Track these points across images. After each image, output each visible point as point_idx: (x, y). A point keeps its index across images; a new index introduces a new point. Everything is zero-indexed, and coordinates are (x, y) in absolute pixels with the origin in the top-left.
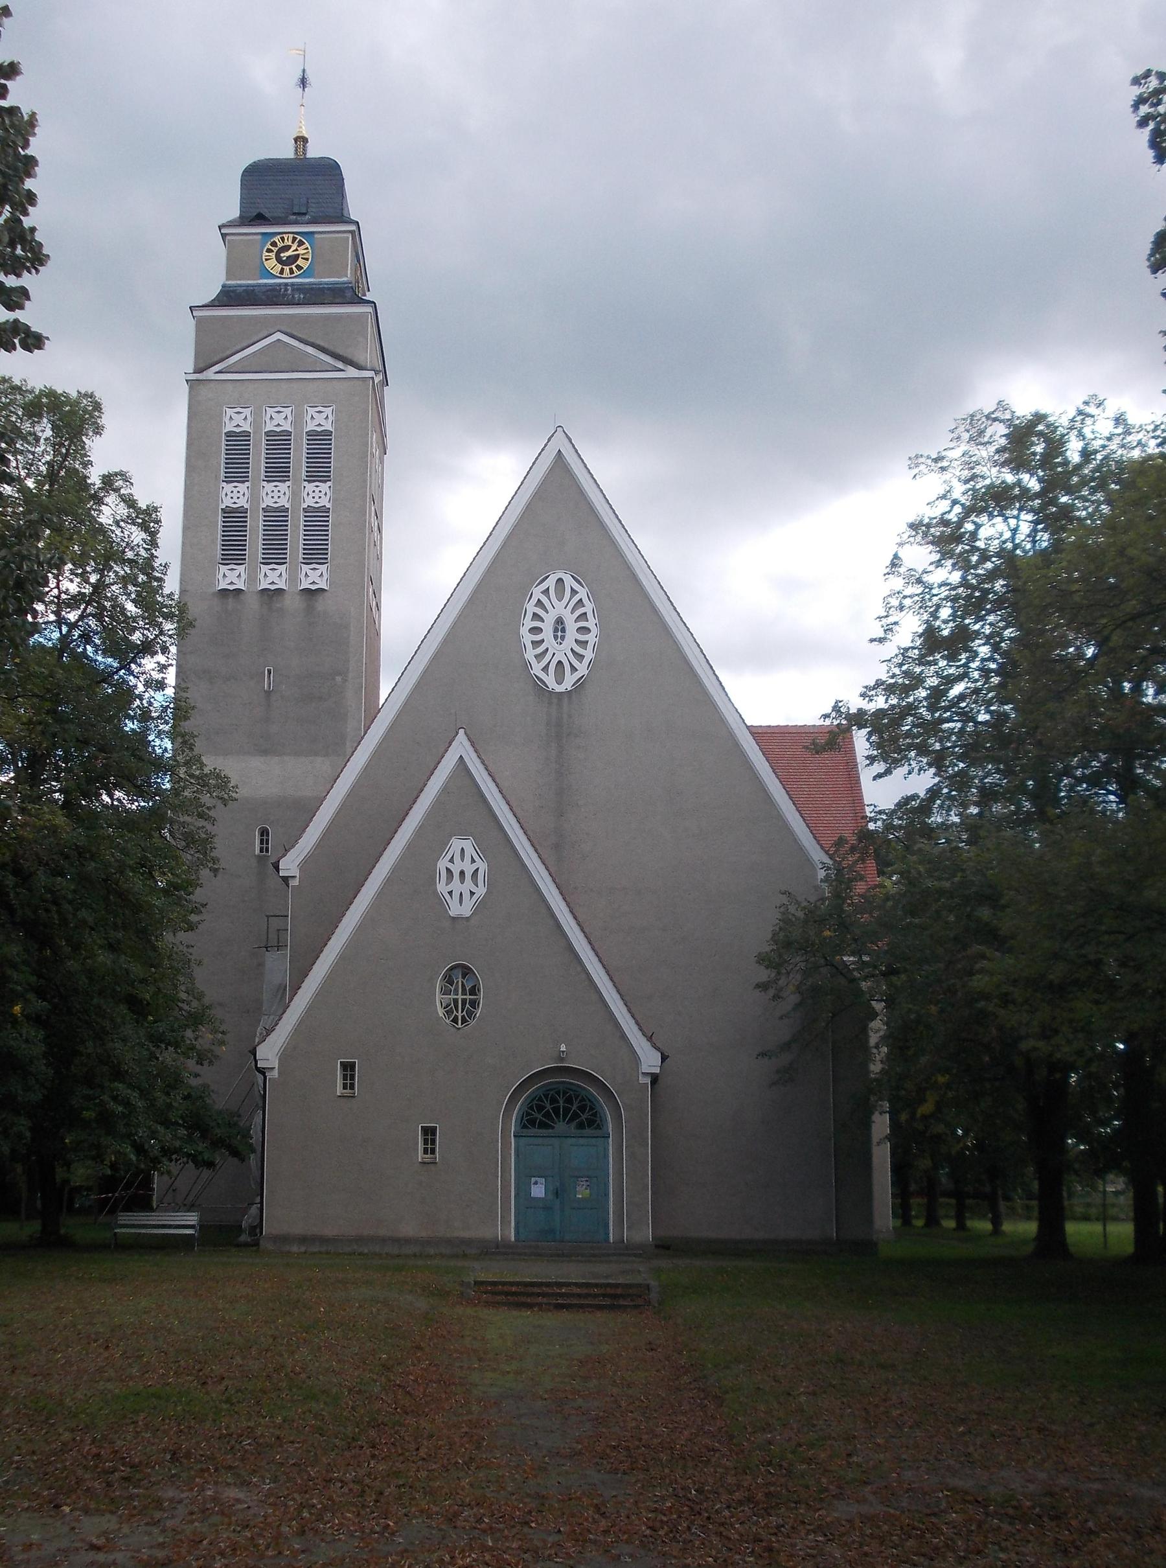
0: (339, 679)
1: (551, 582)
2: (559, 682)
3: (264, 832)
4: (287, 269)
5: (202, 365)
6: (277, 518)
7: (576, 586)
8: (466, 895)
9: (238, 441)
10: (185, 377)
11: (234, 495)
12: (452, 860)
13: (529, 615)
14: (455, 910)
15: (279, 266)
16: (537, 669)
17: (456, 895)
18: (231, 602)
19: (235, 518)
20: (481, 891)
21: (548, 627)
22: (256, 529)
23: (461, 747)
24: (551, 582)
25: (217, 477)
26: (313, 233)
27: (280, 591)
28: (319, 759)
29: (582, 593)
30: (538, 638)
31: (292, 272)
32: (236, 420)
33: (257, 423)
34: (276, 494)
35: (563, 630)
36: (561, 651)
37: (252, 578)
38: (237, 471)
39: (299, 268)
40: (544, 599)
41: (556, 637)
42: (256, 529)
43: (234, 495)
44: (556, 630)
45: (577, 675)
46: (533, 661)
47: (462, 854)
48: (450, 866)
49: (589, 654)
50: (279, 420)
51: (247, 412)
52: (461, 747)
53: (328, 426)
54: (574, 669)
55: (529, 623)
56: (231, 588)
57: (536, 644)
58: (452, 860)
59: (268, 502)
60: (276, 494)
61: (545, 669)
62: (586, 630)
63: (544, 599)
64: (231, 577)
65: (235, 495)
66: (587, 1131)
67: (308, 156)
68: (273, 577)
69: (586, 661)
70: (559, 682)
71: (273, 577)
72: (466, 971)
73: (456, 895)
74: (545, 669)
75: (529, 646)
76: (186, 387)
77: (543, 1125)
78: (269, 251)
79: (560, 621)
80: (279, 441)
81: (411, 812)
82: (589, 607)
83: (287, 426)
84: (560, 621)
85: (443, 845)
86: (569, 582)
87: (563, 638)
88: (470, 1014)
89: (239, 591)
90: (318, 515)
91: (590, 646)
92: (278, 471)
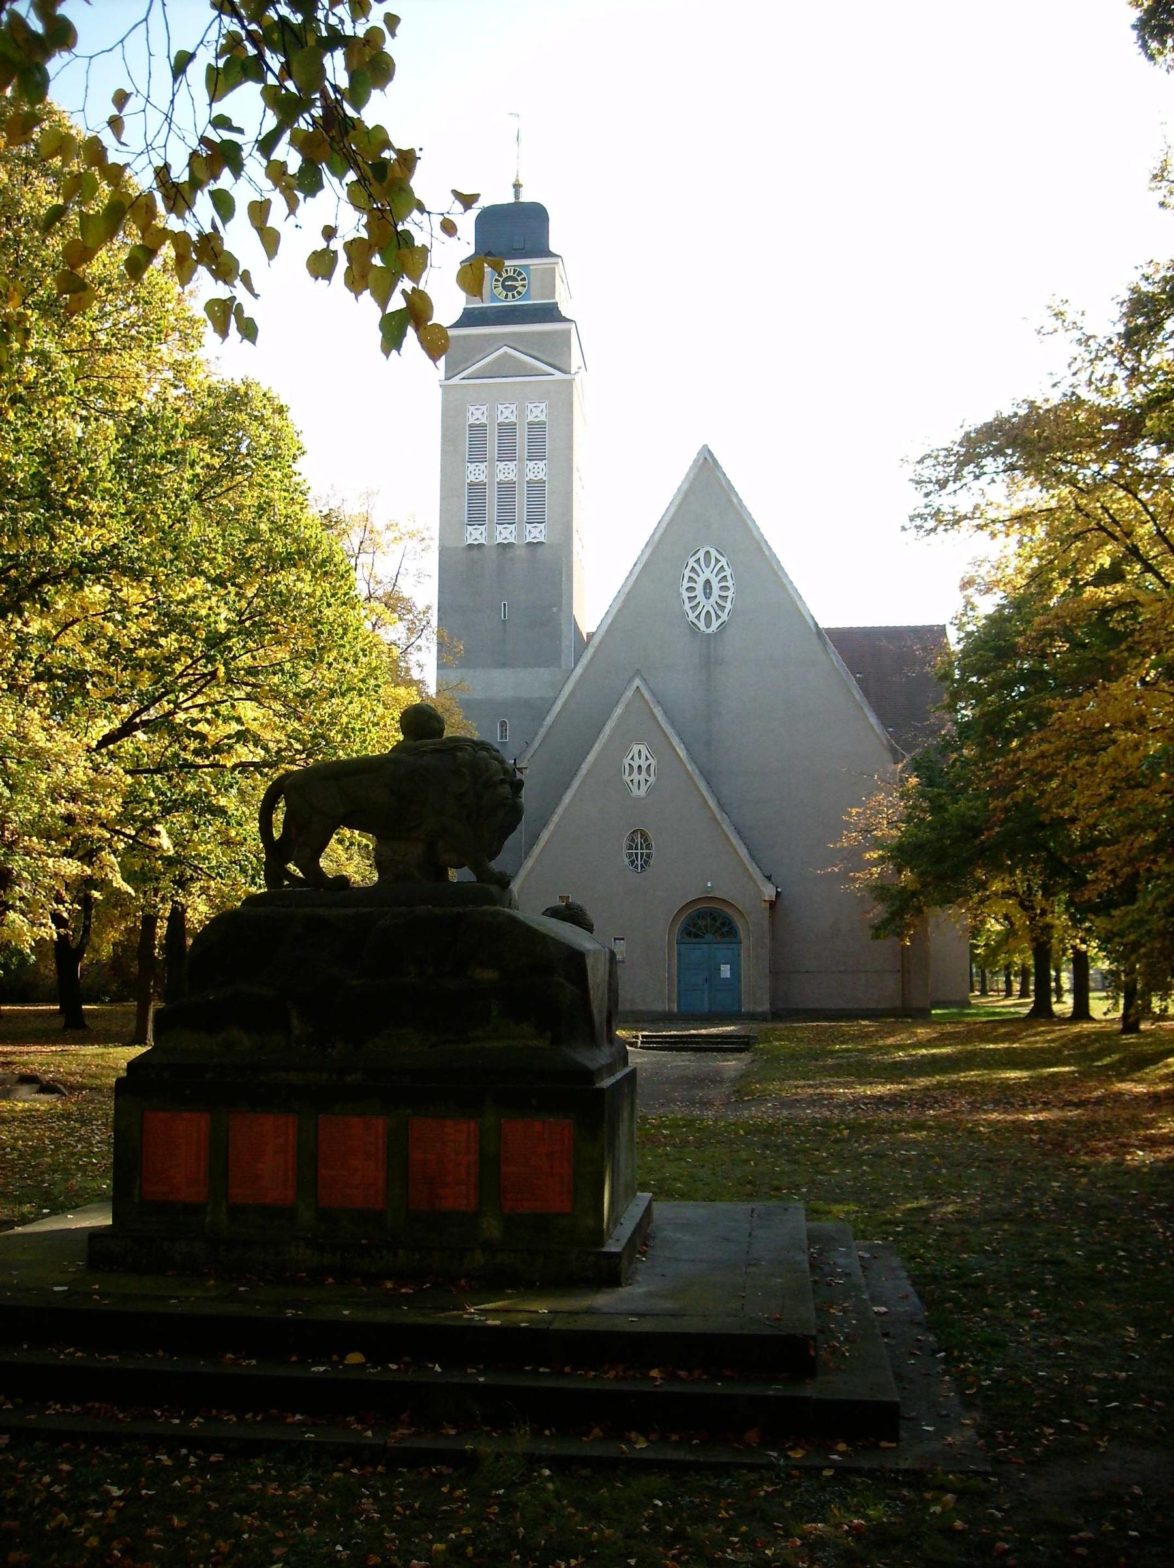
0: (555, 609)
1: (701, 554)
2: (708, 627)
3: (503, 724)
4: (510, 294)
5: (450, 375)
6: (507, 489)
7: (720, 557)
8: (643, 783)
9: (478, 430)
10: (438, 383)
11: (476, 473)
12: (632, 759)
13: (686, 579)
14: (636, 792)
15: (504, 293)
16: (692, 617)
17: (643, 757)
18: (475, 553)
19: (477, 489)
20: (652, 779)
21: (699, 586)
22: (492, 509)
23: (637, 682)
24: (701, 554)
25: (463, 460)
26: (528, 266)
27: (510, 545)
28: (543, 670)
29: (723, 561)
30: (693, 595)
31: (514, 296)
32: (477, 415)
33: (491, 417)
34: (506, 471)
35: (711, 588)
36: (708, 605)
37: (491, 536)
38: (477, 455)
39: (519, 293)
40: (696, 566)
41: (705, 593)
42: (492, 509)
43: (476, 473)
44: (705, 588)
45: (720, 621)
46: (690, 612)
47: (639, 754)
48: (631, 762)
49: (729, 606)
50: (507, 414)
51: (484, 408)
52: (637, 682)
53: (543, 418)
54: (718, 617)
55: (686, 584)
56: (476, 543)
57: (691, 599)
58: (632, 759)
59: (501, 477)
60: (506, 471)
61: (698, 617)
62: (726, 588)
63: (696, 566)
64: (476, 535)
65: (477, 472)
66: (727, 939)
67: (521, 200)
68: (505, 534)
69: (727, 611)
70: (708, 627)
71: (506, 533)
72: (644, 835)
73: (643, 757)
74: (698, 617)
75: (686, 601)
76: (440, 390)
77: (697, 936)
78: (497, 280)
79: (708, 582)
80: (507, 429)
81: (615, 594)
82: (728, 572)
83: (513, 419)
84: (708, 582)
85: (626, 749)
86: (702, 625)
87: (711, 594)
88: (646, 862)
89: (481, 545)
90: (536, 487)
91: (729, 600)
92: (507, 454)
